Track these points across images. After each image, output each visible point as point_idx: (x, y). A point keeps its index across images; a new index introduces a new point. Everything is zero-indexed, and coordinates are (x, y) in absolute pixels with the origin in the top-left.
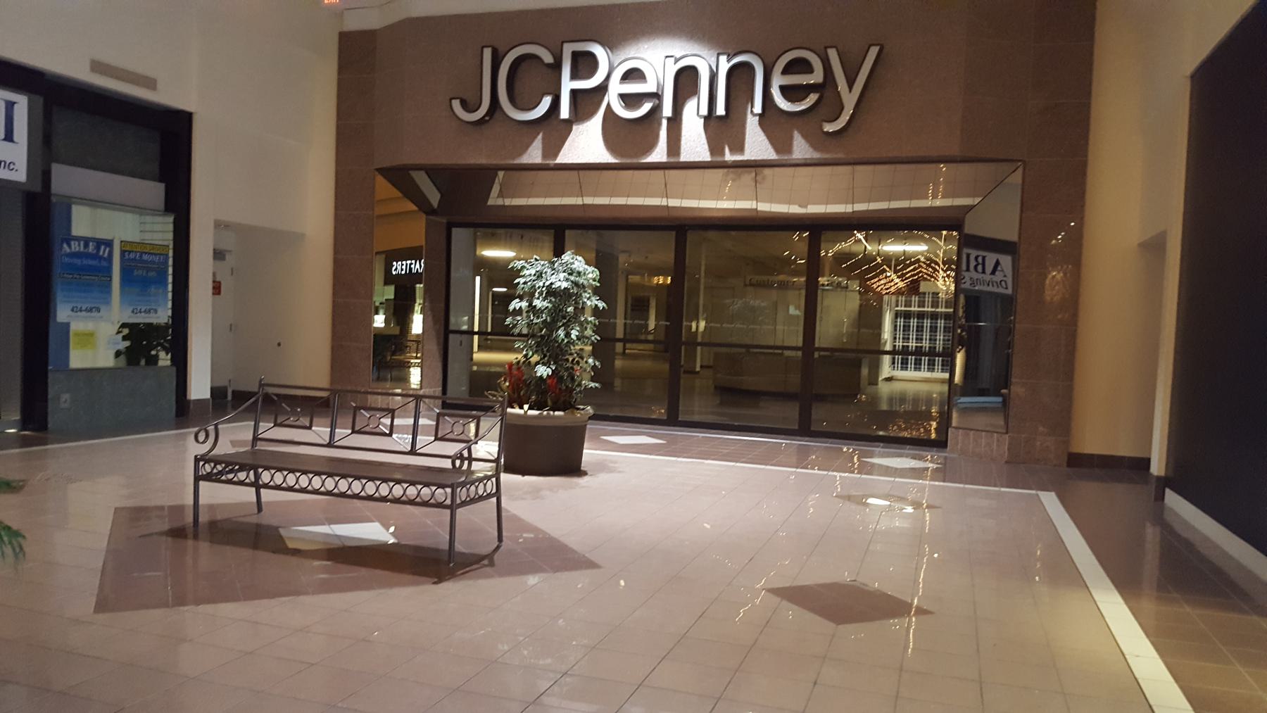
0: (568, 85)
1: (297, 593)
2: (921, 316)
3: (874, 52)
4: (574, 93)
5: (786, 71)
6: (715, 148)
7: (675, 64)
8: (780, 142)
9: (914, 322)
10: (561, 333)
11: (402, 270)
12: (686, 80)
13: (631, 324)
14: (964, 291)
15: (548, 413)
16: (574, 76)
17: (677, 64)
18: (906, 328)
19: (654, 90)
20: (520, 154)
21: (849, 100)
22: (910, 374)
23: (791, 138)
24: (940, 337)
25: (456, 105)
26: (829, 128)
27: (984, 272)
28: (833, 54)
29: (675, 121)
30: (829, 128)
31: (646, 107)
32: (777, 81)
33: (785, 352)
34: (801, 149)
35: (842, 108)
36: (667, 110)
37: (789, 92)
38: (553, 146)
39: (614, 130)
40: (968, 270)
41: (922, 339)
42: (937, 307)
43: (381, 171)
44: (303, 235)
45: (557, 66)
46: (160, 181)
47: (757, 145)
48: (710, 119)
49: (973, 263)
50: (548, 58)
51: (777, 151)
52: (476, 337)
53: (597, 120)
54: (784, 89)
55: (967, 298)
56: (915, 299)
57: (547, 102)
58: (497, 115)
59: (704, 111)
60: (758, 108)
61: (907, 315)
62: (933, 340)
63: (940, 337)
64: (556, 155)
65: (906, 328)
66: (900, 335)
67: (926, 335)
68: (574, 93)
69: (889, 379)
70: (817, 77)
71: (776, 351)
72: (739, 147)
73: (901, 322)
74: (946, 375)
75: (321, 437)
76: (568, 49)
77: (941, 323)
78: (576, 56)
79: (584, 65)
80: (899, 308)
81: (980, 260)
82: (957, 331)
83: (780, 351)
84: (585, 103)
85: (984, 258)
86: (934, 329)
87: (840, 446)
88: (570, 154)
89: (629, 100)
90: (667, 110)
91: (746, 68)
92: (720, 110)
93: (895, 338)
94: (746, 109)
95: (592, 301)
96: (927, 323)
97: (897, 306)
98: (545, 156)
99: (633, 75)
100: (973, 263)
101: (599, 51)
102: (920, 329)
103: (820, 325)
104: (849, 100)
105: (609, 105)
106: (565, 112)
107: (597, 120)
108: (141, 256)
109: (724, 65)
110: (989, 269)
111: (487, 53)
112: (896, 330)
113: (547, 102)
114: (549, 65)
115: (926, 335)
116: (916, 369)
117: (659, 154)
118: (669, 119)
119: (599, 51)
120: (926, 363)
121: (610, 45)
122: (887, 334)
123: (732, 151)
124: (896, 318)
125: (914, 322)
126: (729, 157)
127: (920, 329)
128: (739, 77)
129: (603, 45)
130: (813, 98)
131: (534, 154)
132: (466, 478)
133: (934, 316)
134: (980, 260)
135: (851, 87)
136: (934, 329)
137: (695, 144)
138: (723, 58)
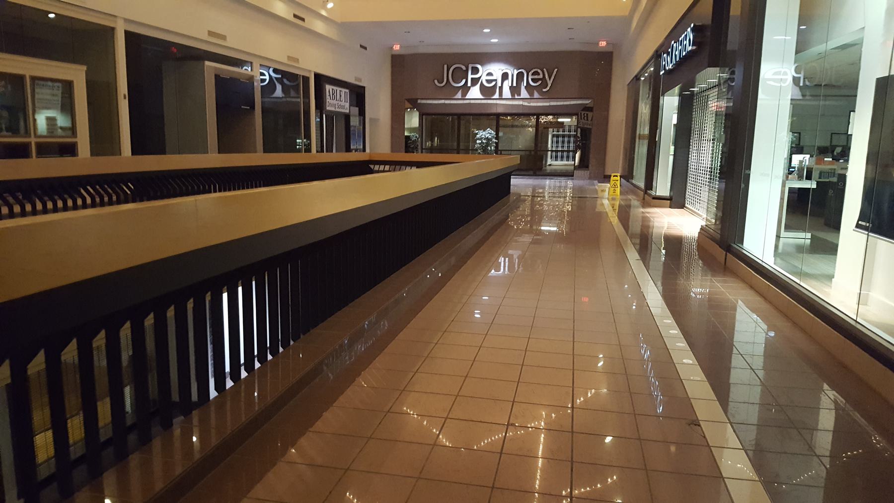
0: (470, 76)
2: (563, 136)
4: (472, 79)
5: (533, 74)
6: (513, 95)
8: (531, 94)
9: (560, 139)
10: (489, 148)
12: (505, 76)
14: (580, 127)
16: (472, 74)
18: (557, 142)
19: (495, 78)
20: (455, 95)
21: (550, 83)
22: (559, 163)
23: (534, 92)
24: (572, 145)
25: (436, 81)
26: (544, 90)
27: (587, 120)
29: (501, 88)
30: (544, 90)
31: (493, 83)
34: (536, 95)
35: (547, 85)
36: (499, 84)
37: (533, 80)
39: (483, 89)
40: (581, 119)
41: (564, 147)
42: (571, 132)
43: (406, 100)
44: (378, 119)
46: (357, 107)
47: (524, 93)
48: (511, 88)
49: (583, 117)
50: (464, 68)
51: (530, 96)
52: (470, 148)
53: (479, 85)
54: (532, 80)
55: (581, 130)
56: (561, 130)
57: (464, 81)
58: (448, 83)
60: (525, 84)
61: (558, 136)
62: (569, 147)
63: (572, 145)
64: (466, 96)
65: (557, 142)
66: (555, 145)
67: (566, 145)
68: (472, 79)
69: (550, 165)
70: (541, 76)
72: (519, 94)
73: (555, 139)
74: (573, 162)
76: (470, 66)
77: (572, 139)
78: (472, 68)
79: (475, 71)
80: (554, 133)
81: (585, 115)
84: (475, 81)
85: (587, 114)
86: (569, 142)
88: (470, 95)
89: (489, 81)
90: (499, 84)
92: (515, 85)
93: (552, 147)
94: (521, 84)
95: (494, 140)
96: (566, 139)
97: (553, 132)
98: (462, 96)
99: (490, 74)
100: (583, 117)
101: (479, 66)
102: (563, 142)
103: (699, 153)
104: (550, 83)
105: (482, 82)
106: (469, 84)
107: (479, 85)
109: (516, 72)
110: (590, 119)
111: (446, 66)
112: (553, 143)
113: (464, 81)
114: (465, 70)
115: (566, 145)
116: (561, 160)
117: (497, 96)
118: (499, 87)
119: (479, 66)
121: (482, 65)
122: (549, 146)
123: (518, 96)
124: (553, 137)
125: (560, 139)
126: (516, 97)
127: (563, 142)
128: (520, 76)
129: (479, 64)
130: (540, 82)
131: (459, 95)
133: (569, 136)
134: (585, 115)
135: (550, 80)
136: (569, 142)
137: (507, 93)
138: (515, 70)
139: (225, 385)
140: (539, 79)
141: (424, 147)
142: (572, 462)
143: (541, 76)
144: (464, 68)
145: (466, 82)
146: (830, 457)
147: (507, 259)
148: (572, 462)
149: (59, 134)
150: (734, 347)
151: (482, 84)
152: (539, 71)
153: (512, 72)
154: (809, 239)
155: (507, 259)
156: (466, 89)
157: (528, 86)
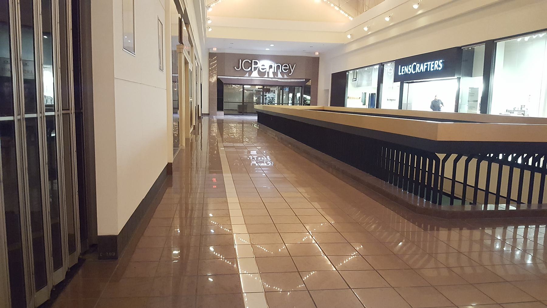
0: (253, 66)
1: (474, 51)
3: (295, 65)
7: (262, 66)
8: (283, 76)
11: (404, 69)
12: (271, 67)
17: (262, 66)
21: (292, 71)
25: (235, 67)
26: (235, 67)
28: (290, 65)
29: (268, 73)
32: (283, 68)
34: (285, 77)
38: (250, 75)
47: (280, 76)
48: (274, 73)
50: (250, 62)
59: (281, 71)
64: (250, 76)
70: (288, 68)
75: (310, 295)
76: (253, 61)
79: (256, 63)
82: (289, 146)
84: (255, 69)
87: (408, 190)
106: (253, 70)
109: (276, 65)
113: (250, 68)
128: (278, 67)
130: (288, 70)
137: (271, 75)
140: (287, 69)
143: (288, 68)
144: (250, 62)
152: (288, 66)
153: (274, 65)
157: (282, 73)
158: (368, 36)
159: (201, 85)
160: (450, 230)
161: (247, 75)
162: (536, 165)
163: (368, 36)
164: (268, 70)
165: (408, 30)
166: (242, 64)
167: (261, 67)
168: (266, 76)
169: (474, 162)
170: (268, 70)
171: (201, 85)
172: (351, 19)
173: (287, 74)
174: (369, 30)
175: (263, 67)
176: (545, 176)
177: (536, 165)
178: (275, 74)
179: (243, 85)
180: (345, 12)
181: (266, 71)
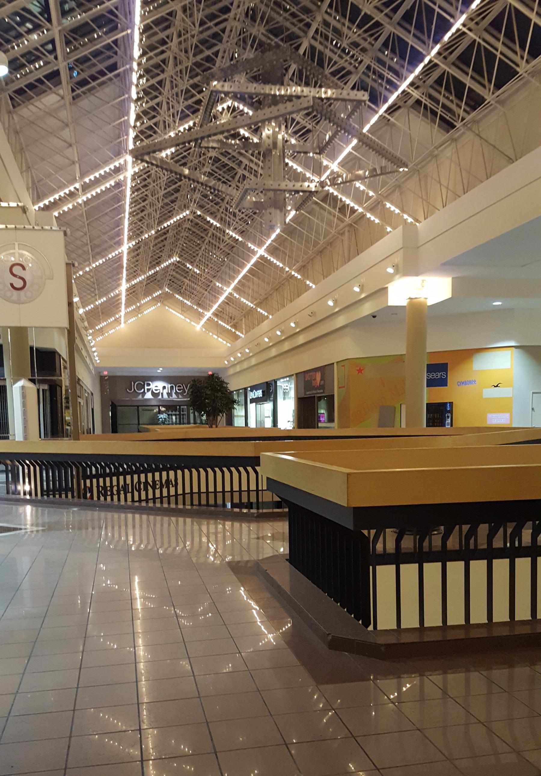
0: (146, 387)
12: (164, 388)
13: (252, 508)
15: (300, 213)
21: (187, 391)
25: (128, 390)
26: (128, 390)
29: (162, 394)
33: (130, 494)
34: (180, 396)
37: (178, 390)
38: (143, 396)
39: (153, 393)
45: (144, 385)
47: (174, 396)
48: (168, 394)
50: (143, 384)
57: (143, 390)
71: (45, 478)
76: (146, 383)
79: (149, 385)
83: (130, 491)
84: (148, 390)
91: (173, 386)
101: (150, 383)
104: (187, 391)
106: (146, 391)
108: (45, 491)
109: (169, 386)
113: (143, 390)
119: (150, 383)
120: (447, 113)
128: (172, 388)
132: (388, 704)
137: (165, 396)
139: (469, 529)
141: (260, 488)
142: (216, 753)
143: (182, 388)
144: (143, 384)
145: (144, 390)
146: (445, 672)
147: (89, 473)
148: (216, 753)
149: (382, 545)
150: (502, 529)
151: (152, 392)
154: (467, 681)
155: (89, 473)
156: (144, 393)
157: (176, 393)
158: (333, 315)
159: (93, 410)
160: (399, 677)
161: (140, 397)
162: (517, 545)
163: (333, 315)
164: (161, 391)
165: (262, 360)
166: (134, 386)
167: (154, 388)
168: (160, 397)
169: (179, 472)
170: (161, 391)
171: (93, 410)
172: (229, 345)
173: (182, 394)
174: (362, 291)
175: (156, 388)
176: (507, 558)
177: (517, 545)
178: (169, 394)
179: (138, 406)
180: (223, 340)
181: (159, 393)
